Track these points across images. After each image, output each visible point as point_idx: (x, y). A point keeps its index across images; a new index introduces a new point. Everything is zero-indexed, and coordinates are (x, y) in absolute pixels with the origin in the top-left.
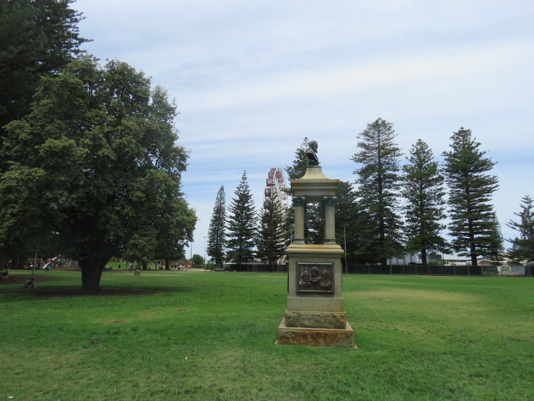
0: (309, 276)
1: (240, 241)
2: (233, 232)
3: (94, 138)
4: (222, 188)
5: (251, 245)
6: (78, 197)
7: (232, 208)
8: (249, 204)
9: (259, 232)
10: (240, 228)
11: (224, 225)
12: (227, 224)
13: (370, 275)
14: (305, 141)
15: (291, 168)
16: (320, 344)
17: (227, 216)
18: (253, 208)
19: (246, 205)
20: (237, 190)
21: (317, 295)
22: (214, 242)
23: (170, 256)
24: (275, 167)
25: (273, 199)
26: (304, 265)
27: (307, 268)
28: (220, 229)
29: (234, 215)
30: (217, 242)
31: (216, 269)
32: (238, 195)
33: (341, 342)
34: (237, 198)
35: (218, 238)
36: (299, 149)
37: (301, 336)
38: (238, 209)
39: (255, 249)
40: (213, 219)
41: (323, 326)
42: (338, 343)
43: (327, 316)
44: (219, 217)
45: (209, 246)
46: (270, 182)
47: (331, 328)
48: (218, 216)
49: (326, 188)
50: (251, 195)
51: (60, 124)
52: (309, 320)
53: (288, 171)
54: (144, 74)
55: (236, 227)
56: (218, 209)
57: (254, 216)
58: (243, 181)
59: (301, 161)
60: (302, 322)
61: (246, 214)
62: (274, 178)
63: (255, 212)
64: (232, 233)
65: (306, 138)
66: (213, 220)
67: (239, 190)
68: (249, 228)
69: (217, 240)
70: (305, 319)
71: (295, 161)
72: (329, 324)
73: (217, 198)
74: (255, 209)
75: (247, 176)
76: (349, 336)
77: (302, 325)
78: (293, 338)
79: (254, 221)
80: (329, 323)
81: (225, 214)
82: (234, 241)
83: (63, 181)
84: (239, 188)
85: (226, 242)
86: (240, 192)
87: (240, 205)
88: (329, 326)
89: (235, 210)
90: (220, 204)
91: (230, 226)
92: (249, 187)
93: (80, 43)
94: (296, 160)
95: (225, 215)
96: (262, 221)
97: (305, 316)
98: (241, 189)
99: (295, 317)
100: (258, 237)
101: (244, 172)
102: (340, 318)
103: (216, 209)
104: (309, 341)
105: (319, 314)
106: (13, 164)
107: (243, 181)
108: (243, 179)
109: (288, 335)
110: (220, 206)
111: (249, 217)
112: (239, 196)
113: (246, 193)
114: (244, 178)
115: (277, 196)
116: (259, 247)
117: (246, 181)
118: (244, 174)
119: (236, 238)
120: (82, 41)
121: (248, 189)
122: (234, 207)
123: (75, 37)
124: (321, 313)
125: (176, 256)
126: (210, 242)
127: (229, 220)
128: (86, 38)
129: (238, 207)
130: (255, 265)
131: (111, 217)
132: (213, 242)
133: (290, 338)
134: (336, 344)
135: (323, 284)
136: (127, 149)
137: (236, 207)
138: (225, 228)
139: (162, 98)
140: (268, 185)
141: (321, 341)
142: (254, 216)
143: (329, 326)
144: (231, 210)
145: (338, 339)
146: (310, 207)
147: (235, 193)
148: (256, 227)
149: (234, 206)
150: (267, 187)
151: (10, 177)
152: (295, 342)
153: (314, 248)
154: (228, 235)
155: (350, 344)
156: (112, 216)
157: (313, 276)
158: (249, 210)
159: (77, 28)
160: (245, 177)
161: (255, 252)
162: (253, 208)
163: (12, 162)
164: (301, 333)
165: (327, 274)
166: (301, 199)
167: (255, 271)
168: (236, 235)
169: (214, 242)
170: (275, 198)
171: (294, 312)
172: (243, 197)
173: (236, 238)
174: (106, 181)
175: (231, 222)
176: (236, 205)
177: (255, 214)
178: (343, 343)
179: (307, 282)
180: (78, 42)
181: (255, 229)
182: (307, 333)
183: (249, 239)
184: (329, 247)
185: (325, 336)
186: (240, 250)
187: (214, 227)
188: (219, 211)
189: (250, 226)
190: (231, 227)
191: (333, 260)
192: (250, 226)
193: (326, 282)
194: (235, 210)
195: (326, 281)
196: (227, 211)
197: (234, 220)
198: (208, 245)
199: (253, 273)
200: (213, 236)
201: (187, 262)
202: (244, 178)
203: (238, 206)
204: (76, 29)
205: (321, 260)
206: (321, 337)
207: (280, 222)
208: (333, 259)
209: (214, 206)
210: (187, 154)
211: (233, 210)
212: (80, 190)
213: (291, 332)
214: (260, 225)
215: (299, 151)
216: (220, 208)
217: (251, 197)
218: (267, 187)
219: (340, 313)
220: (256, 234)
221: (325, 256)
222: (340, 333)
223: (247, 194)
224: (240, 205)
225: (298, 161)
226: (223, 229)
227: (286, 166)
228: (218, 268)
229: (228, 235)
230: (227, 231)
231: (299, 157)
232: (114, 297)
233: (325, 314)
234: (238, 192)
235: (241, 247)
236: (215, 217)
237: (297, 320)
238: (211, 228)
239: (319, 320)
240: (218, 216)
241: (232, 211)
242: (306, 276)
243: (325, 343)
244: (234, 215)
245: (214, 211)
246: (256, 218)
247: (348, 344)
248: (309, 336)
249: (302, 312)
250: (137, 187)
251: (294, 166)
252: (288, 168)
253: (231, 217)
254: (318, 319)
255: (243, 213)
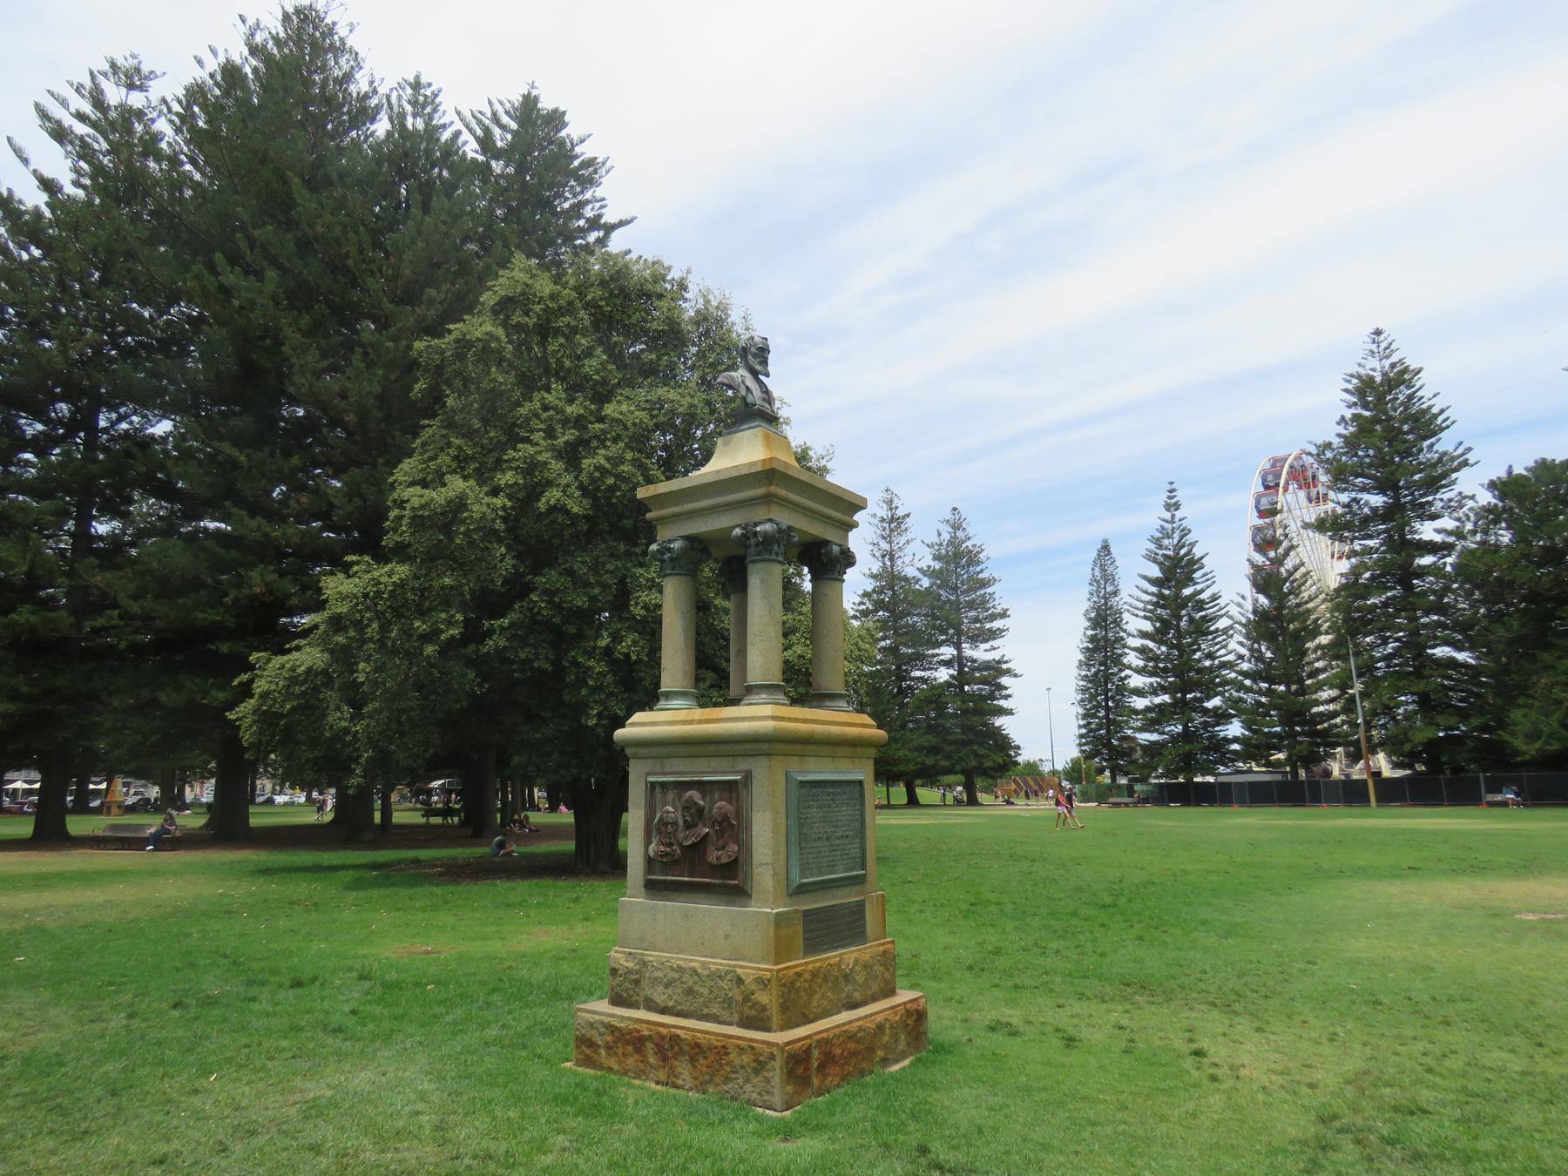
0: (675, 823)
1: (1180, 708)
2: (1153, 680)
3: (532, 467)
4: (1106, 548)
5: (1222, 717)
6: (512, 624)
7: (1141, 605)
8: (1198, 587)
9: (1241, 673)
10: (1174, 666)
11: (1125, 661)
12: (1133, 659)
13: (1448, 809)
14: (1374, 342)
15: (1328, 445)
16: (680, 1082)
17: (1129, 635)
18: (1215, 598)
19: (1187, 592)
20: (1153, 547)
21: (702, 896)
22: (1098, 718)
23: (973, 763)
24: (1280, 453)
25: (1279, 561)
26: (663, 785)
27: (671, 796)
28: (1112, 674)
29: (1147, 626)
30: (1107, 717)
31: (1111, 800)
32: (1155, 561)
33: (741, 1081)
34: (1155, 572)
35: (1110, 704)
36: (1352, 376)
37: (627, 1043)
38: (1163, 607)
39: (1235, 729)
40: (1086, 645)
41: (706, 1011)
42: (730, 1086)
43: (720, 977)
44: (1106, 638)
45: (1084, 731)
46: (1265, 504)
47: (730, 1024)
48: (1100, 633)
49: (739, 496)
50: (1202, 558)
51: (459, 448)
52: (666, 986)
53: (1318, 455)
54: (669, 268)
55: (1161, 665)
56: (1098, 614)
57: (1222, 623)
58: (1168, 516)
59: (1367, 414)
60: (648, 991)
61: (1191, 620)
62: (1281, 489)
63: (1221, 609)
64: (1151, 684)
65: (1378, 332)
66: (1087, 649)
67: (1160, 547)
68: (1207, 663)
69: (1108, 709)
70: (655, 981)
71: (1343, 418)
72: (723, 1009)
73: (1094, 581)
74: (1222, 602)
75: (1180, 496)
76: (766, 1063)
77: (651, 1006)
78: (609, 1048)
79: (1219, 639)
80: (724, 1002)
81: (1125, 627)
82: (1160, 708)
83: (452, 587)
84: (1158, 542)
85: (1136, 712)
86: (1161, 552)
87: (1167, 592)
88: (725, 1015)
89: (1150, 611)
90: (1105, 598)
91: (1141, 663)
92: (1190, 531)
93: (607, 235)
94: (1348, 414)
95: (1125, 631)
96: (1247, 636)
97: (658, 969)
98: (1166, 542)
99: (630, 971)
100: (1238, 691)
101: (1169, 487)
102: (753, 987)
103: (1093, 615)
104: (651, 1067)
105: (694, 964)
106: (358, 563)
107: (1168, 516)
108: (1168, 510)
109: (594, 1032)
110: (1106, 603)
111: (1201, 628)
112: (1160, 564)
113: (1183, 552)
114: (1172, 506)
115: (1292, 547)
116: (1247, 725)
117: (1179, 514)
118: (1171, 491)
119: (1166, 698)
120: (610, 229)
121: (1190, 538)
122: (1149, 602)
123: (594, 223)
124: (703, 963)
125: (990, 764)
126: (1085, 716)
127: (1136, 642)
128: (624, 218)
129: (1161, 601)
130: (1238, 784)
131: (590, 668)
132: (1094, 716)
133: (599, 1046)
134: (726, 1088)
135: (713, 856)
136: (610, 481)
137: (1155, 599)
138: (1127, 672)
139: (720, 322)
140: (1262, 514)
141: (684, 1069)
142: (1222, 623)
143: (725, 1015)
144: (1136, 612)
145: (728, 1069)
146: (1422, 572)
147: (1148, 558)
148: (1231, 657)
149: (1148, 598)
150: (1260, 522)
151: (341, 593)
152: (613, 1063)
153: (691, 722)
154: (1139, 692)
155: (768, 1093)
156: (592, 663)
157: (688, 826)
158: (1200, 605)
159: (603, 199)
160: (1173, 501)
161: (1235, 740)
162: (1215, 598)
163: (354, 558)
164: (630, 1032)
165: (726, 818)
166: (669, 550)
167: (1242, 802)
168: (1163, 689)
169: (1098, 718)
170: (1287, 554)
171: (630, 954)
172: (1176, 566)
173: (1166, 698)
174: (570, 572)
175: (1142, 651)
176: (1152, 594)
177: (1221, 616)
178: (745, 1088)
179: (670, 845)
180: (601, 234)
181: (1224, 665)
182: (646, 1033)
183: (1208, 698)
184: (743, 715)
185: (697, 1051)
186: (1186, 736)
187: (1093, 670)
188: (1104, 619)
189: (1210, 656)
190: (1146, 666)
191: (743, 765)
192: (1210, 656)
193: (723, 848)
194: (1150, 611)
195: (720, 843)
196: (1126, 616)
197: (1151, 644)
198: (1080, 727)
199: (1236, 809)
200: (1093, 697)
201: (1043, 779)
202: (1172, 506)
203: (1160, 596)
204: (598, 205)
205: (714, 763)
206: (682, 1052)
207: (1315, 632)
208: (750, 760)
209: (1086, 605)
210: (823, 463)
211: (1145, 610)
212: (516, 606)
213: (602, 1023)
214: (1243, 651)
215: (1355, 381)
216: (1107, 609)
217: (1203, 561)
218: (1260, 522)
219: (759, 969)
220: (1232, 682)
221: (724, 748)
222: (738, 1046)
223: (1186, 555)
224: (1167, 592)
225: (1356, 417)
226: (1123, 675)
227: (1310, 442)
228: (1118, 796)
229: (1139, 692)
230: (1137, 681)
231: (1355, 404)
232: (561, 883)
233: (713, 968)
234: (1156, 554)
235: (1186, 727)
236: (1092, 639)
237: (637, 982)
238: (1084, 673)
239: (697, 988)
240: (1100, 633)
241: (1142, 614)
242: (667, 824)
243: (696, 1078)
244: (1147, 626)
245: (1090, 619)
246: (1225, 631)
247: (760, 1094)
248: (649, 1045)
249: (652, 956)
250: (648, 580)
251: (1339, 435)
252: (1318, 447)
253: (1144, 635)
254: (690, 983)
255: (1179, 618)
